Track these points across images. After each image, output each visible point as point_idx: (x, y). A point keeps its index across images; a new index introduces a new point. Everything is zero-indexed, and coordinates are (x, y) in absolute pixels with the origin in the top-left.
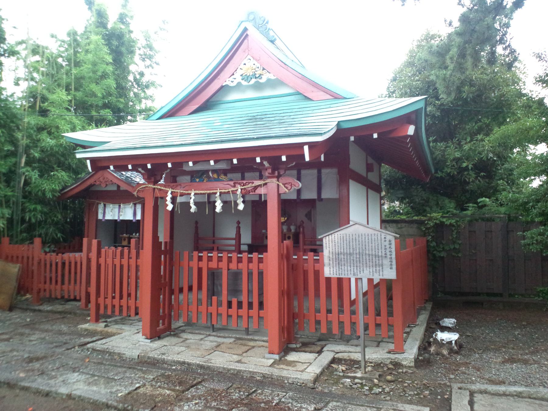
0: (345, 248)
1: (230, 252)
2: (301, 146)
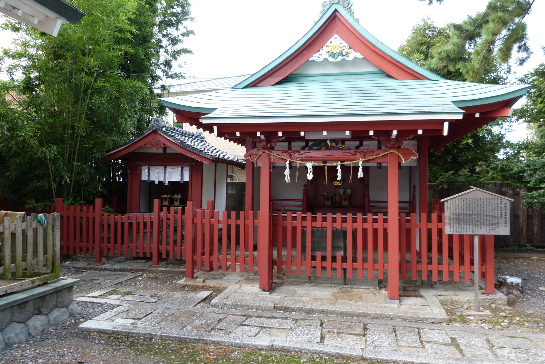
0: (465, 209)
1: (294, 212)
2: (442, 122)
